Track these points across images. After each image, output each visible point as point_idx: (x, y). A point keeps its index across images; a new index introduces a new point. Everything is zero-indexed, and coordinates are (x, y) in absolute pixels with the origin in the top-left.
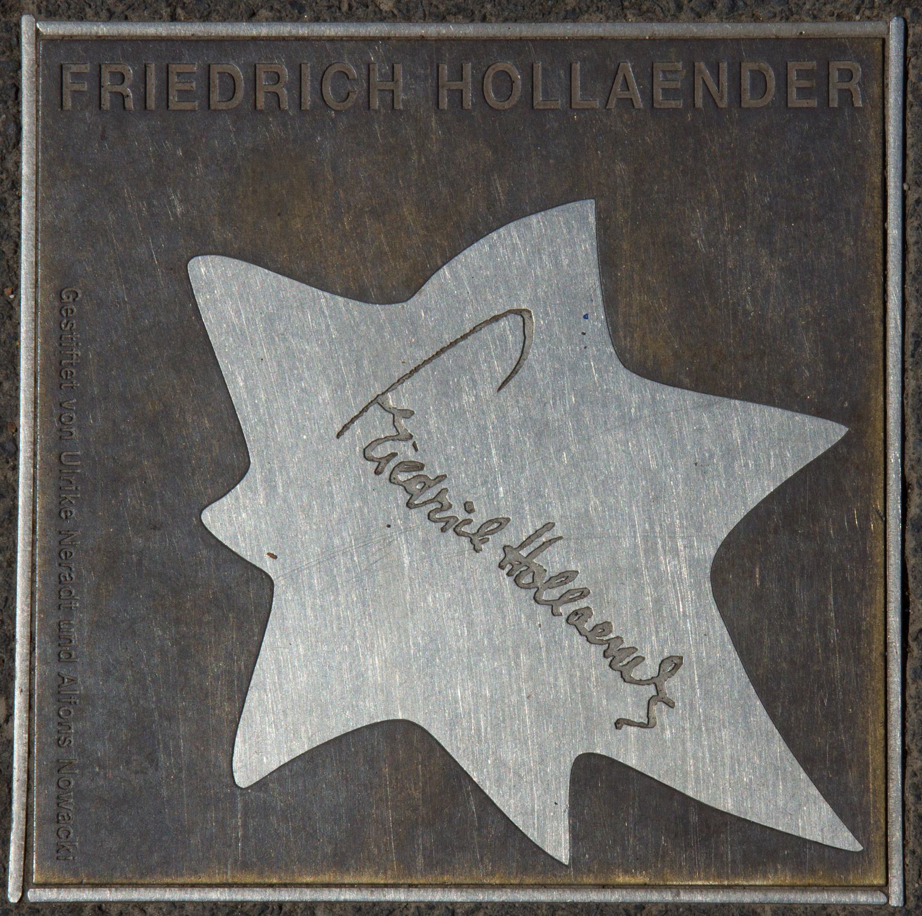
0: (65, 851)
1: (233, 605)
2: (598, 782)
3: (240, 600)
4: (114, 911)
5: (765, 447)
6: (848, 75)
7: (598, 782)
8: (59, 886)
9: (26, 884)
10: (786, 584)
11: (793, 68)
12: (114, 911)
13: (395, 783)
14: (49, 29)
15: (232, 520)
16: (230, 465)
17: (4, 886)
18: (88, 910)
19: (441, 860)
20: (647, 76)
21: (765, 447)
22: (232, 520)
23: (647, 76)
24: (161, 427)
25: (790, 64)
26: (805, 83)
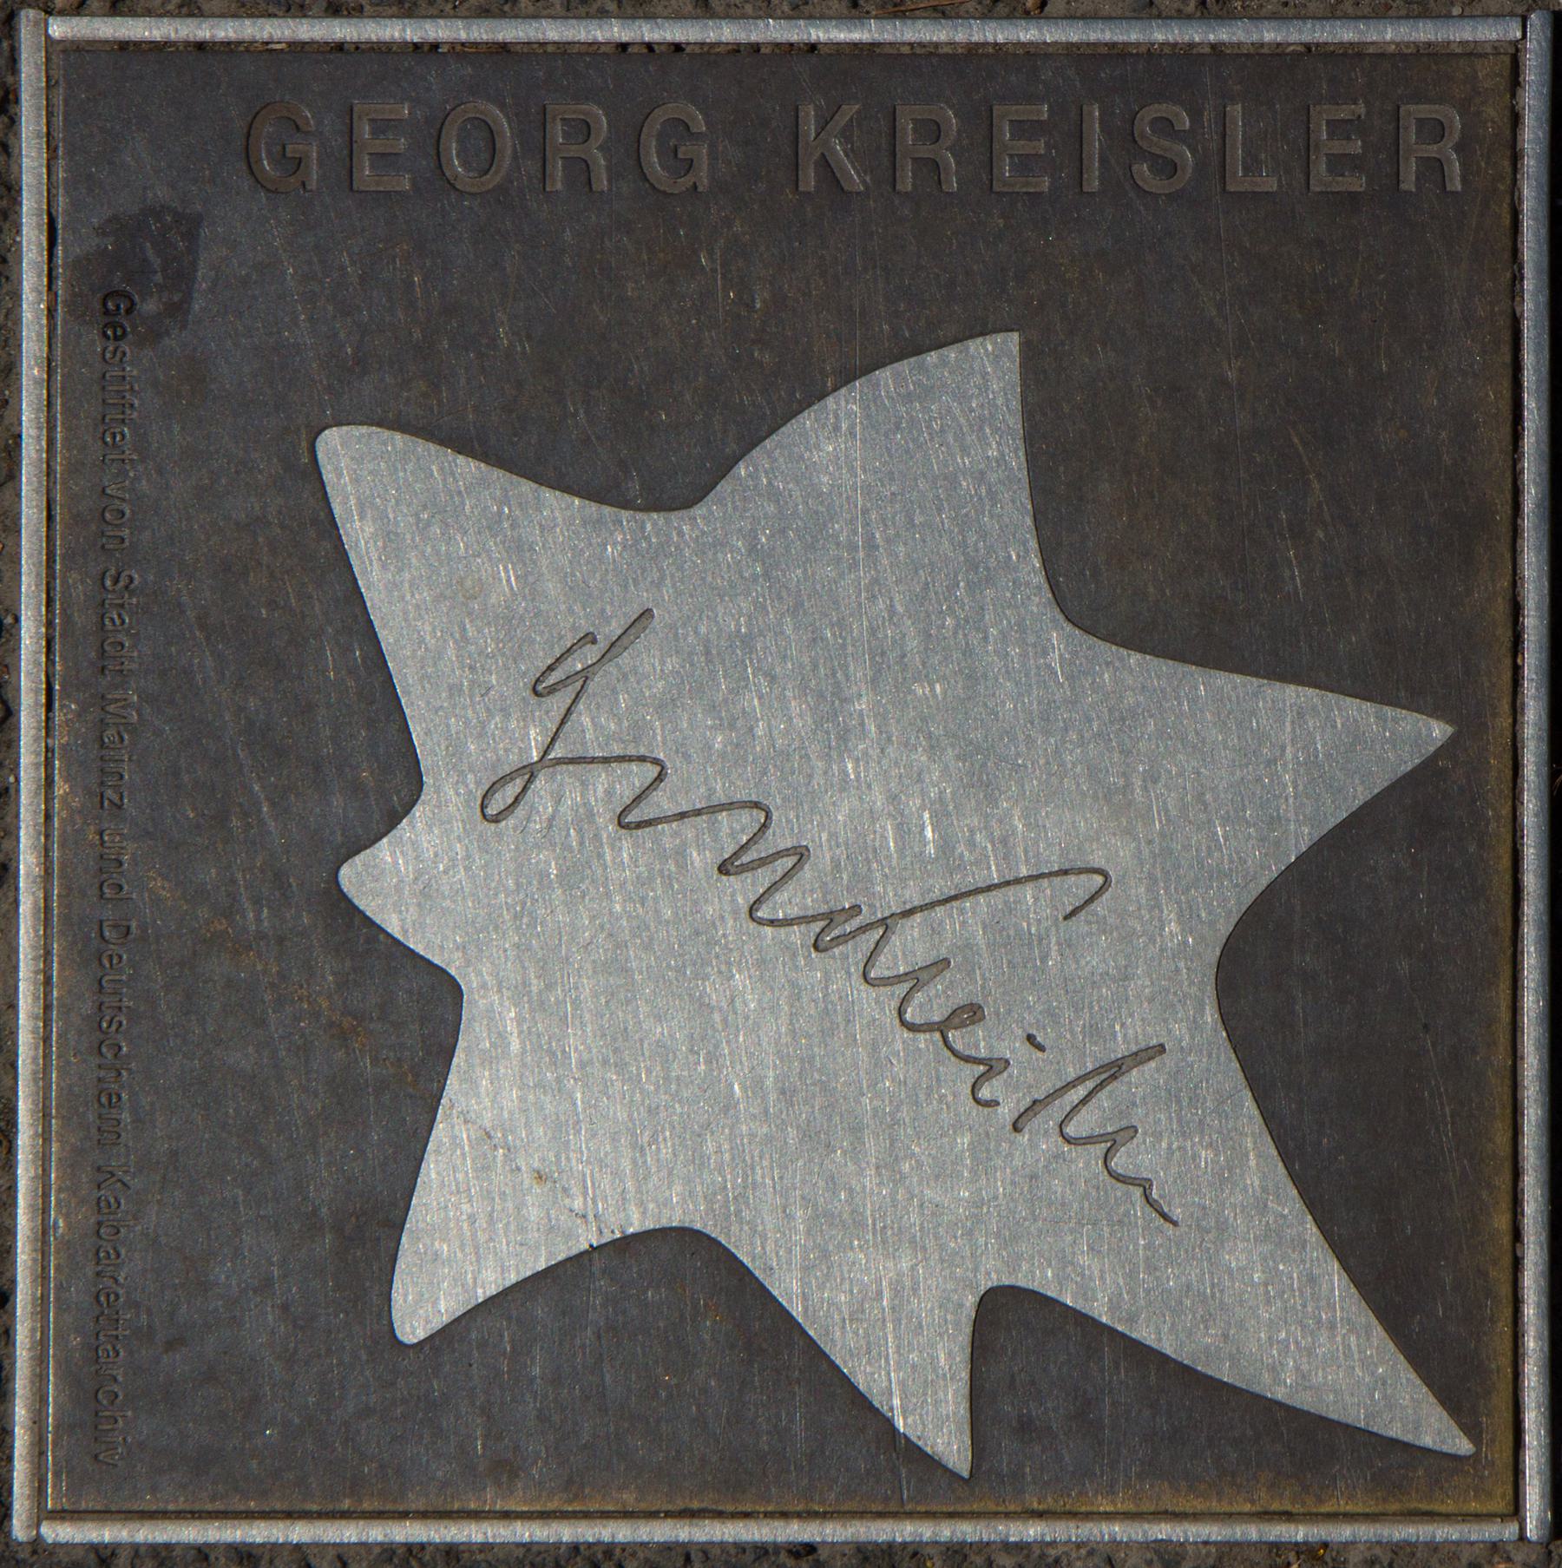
0: (96, 1460)
1: (396, 1030)
2: (1013, 1330)
3: (406, 1021)
4: (1354, 1558)
5: (1296, 756)
6: (1436, 131)
7: (1013, 1330)
8: (544, 1516)
9: (42, 1514)
10: (1341, 1008)
11: (1006, 116)
12: (1354, 1558)
13: (677, 1343)
14: (58, 29)
15: (407, 880)
16: (391, 786)
17: (7, 1515)
18: (122, 1560)
19: (736, 1484)
20: (981, 121)
21: (1296, 756)
22: (407, 880)
23: (981, 121)
24: (254, 722)
25: (997, 110)
26: (1023, 147)
